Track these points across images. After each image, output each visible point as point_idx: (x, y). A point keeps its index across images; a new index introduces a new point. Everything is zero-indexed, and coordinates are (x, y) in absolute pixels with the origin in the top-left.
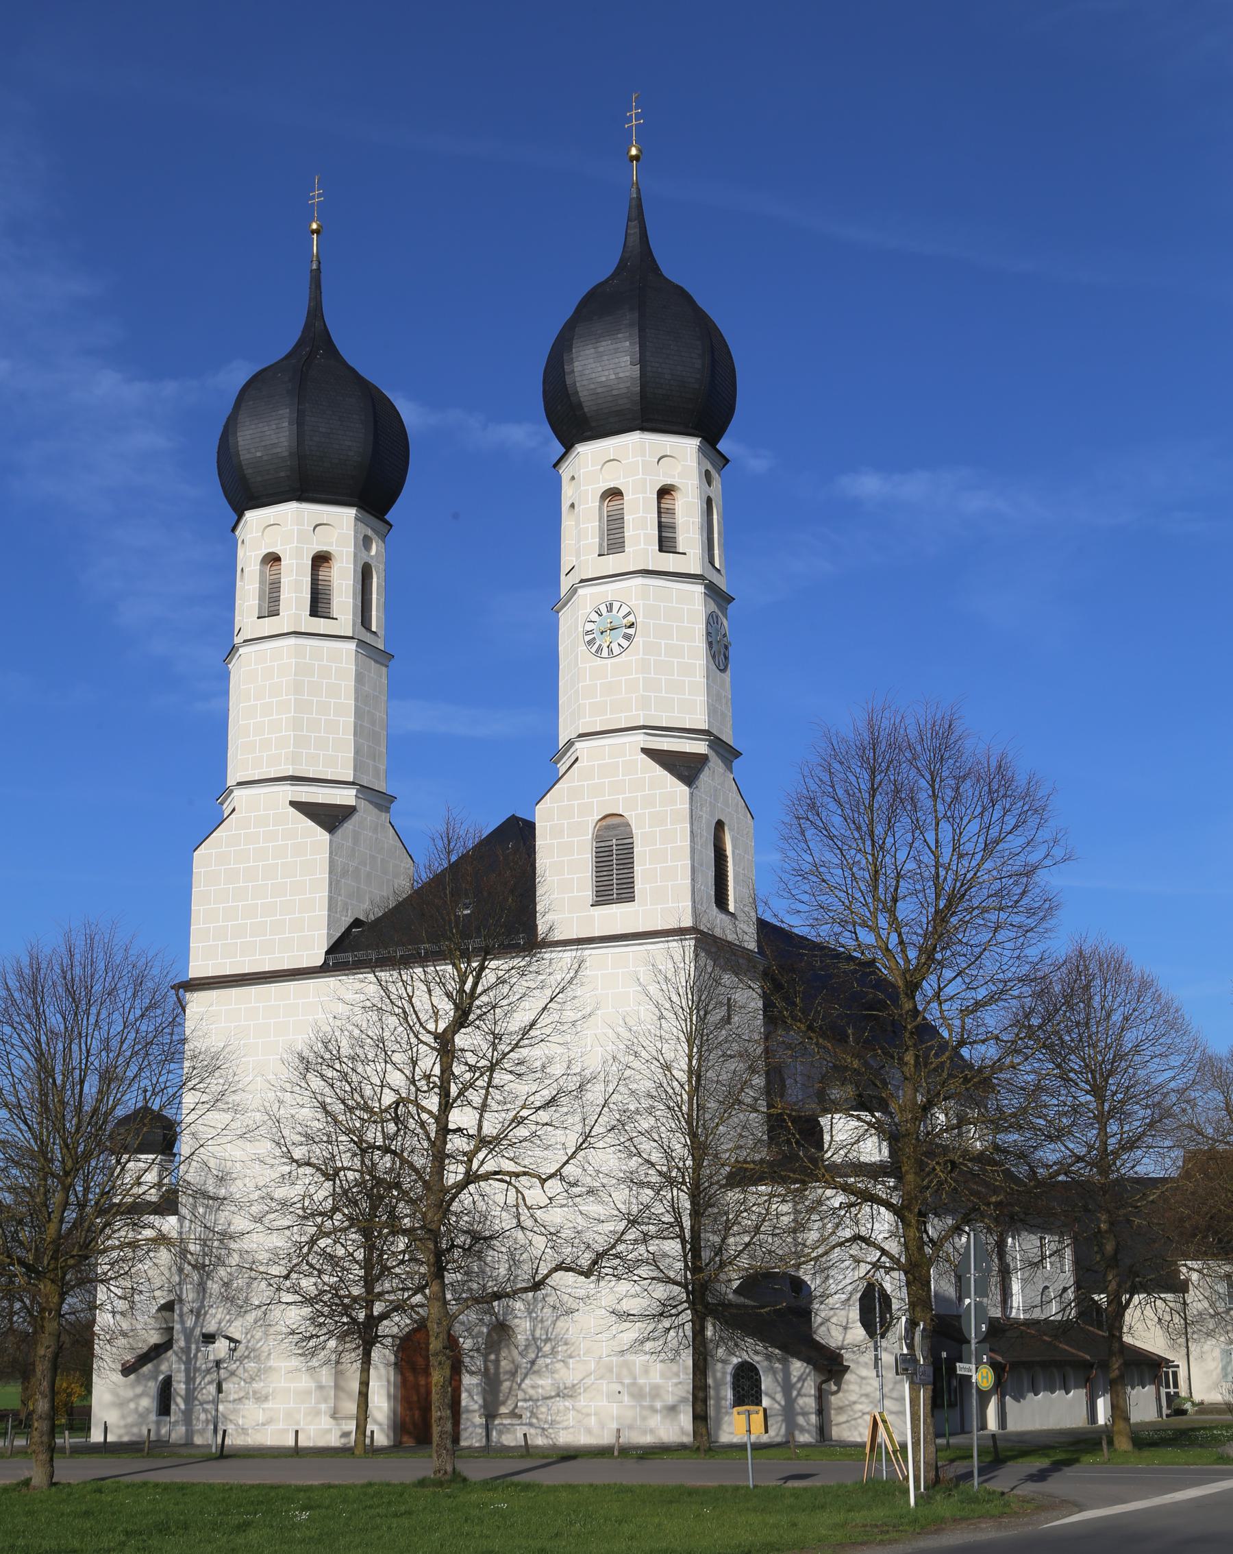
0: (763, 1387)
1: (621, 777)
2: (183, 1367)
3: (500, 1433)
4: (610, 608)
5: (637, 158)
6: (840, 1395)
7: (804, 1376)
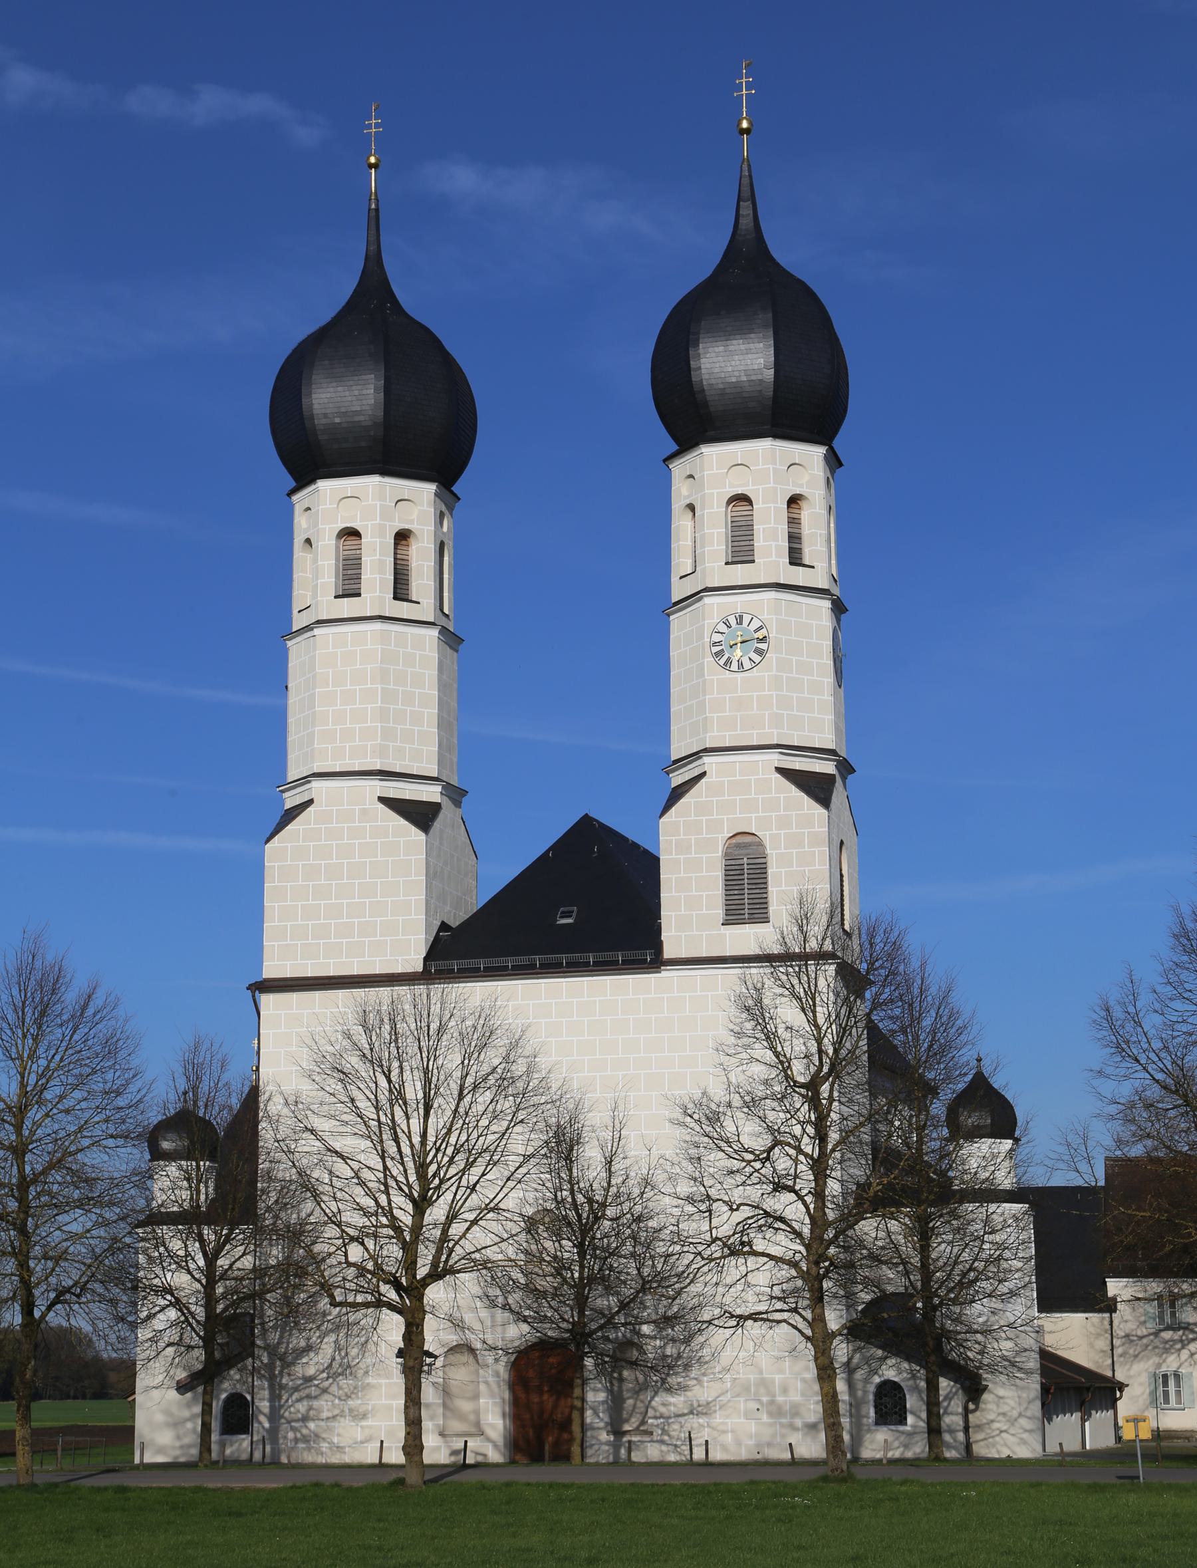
0: (908, 1406)
1: (753, 796)
2: (266, 1384)
4: (740, 620)
6: (978, 1413)
7: (951, 1395)
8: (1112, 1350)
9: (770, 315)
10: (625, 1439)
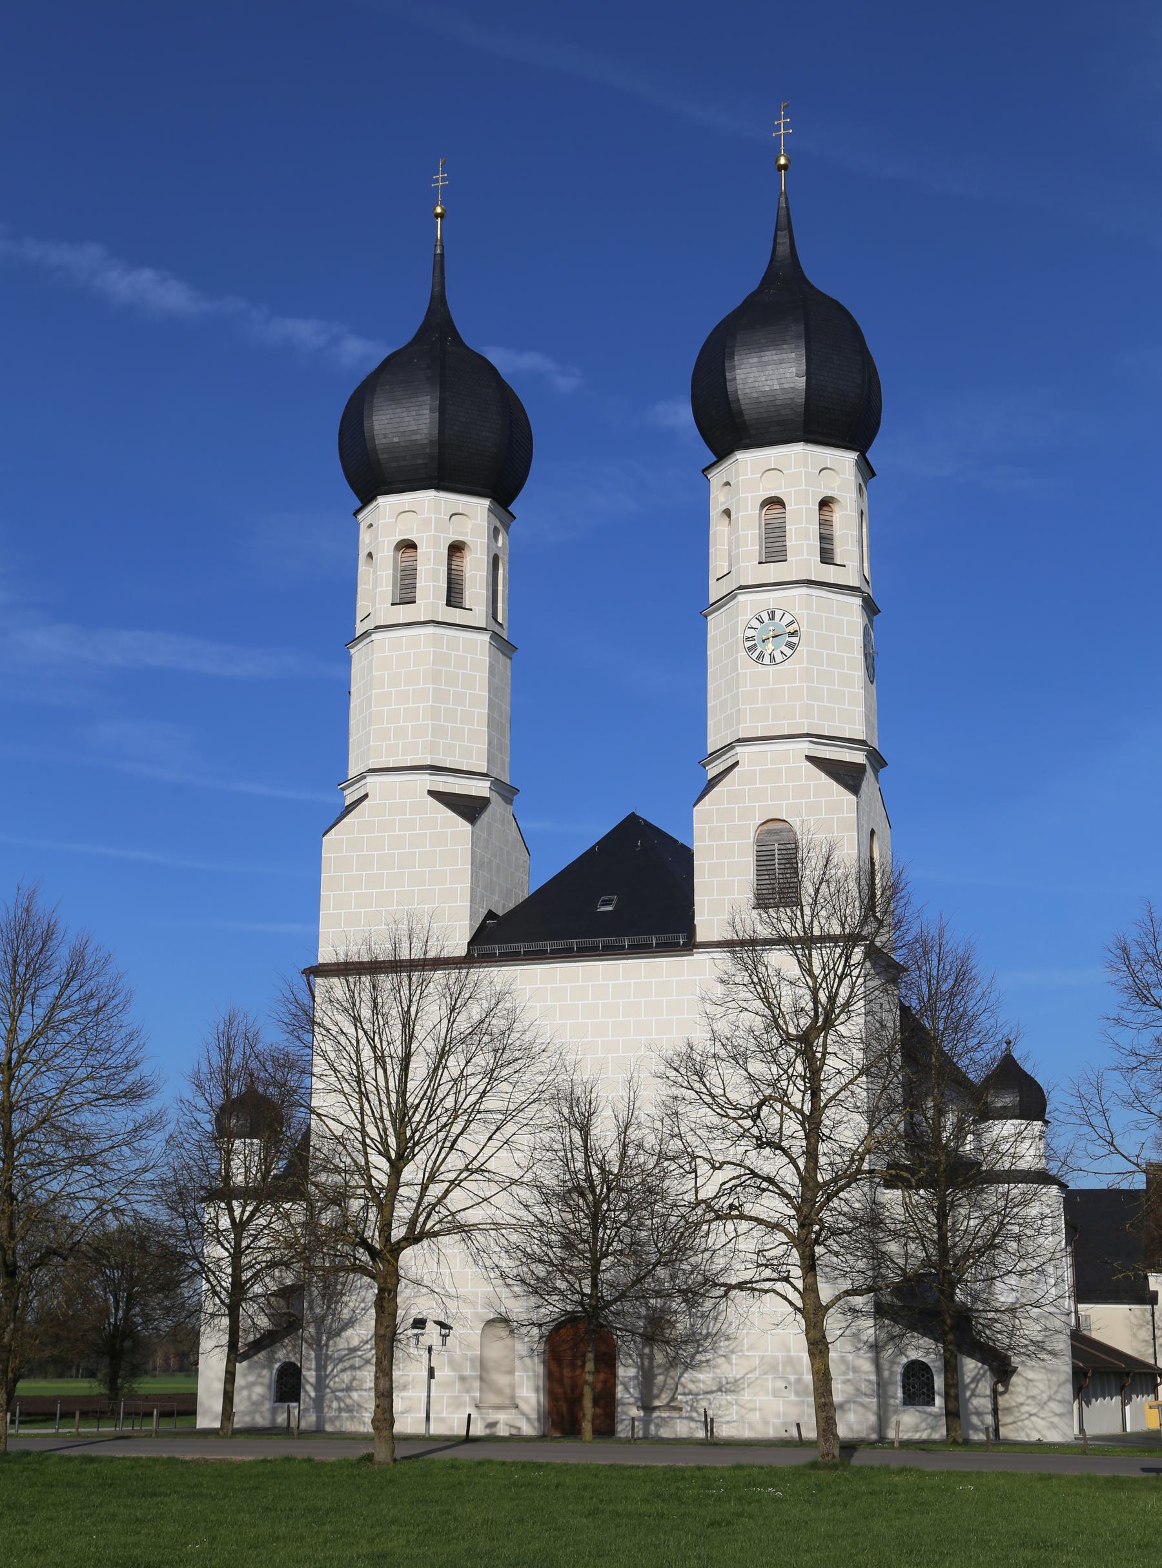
1: (784, 783)
3: (658, 1426)
4: (772, 616)
5: (785, 167)
6: (1007, 1396)
7: (979, 1377)
8: (1154, 1339)
9: (803, 327)
10: (655, 1415)
